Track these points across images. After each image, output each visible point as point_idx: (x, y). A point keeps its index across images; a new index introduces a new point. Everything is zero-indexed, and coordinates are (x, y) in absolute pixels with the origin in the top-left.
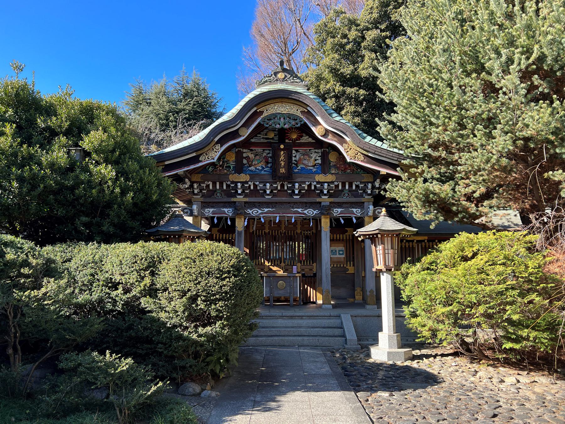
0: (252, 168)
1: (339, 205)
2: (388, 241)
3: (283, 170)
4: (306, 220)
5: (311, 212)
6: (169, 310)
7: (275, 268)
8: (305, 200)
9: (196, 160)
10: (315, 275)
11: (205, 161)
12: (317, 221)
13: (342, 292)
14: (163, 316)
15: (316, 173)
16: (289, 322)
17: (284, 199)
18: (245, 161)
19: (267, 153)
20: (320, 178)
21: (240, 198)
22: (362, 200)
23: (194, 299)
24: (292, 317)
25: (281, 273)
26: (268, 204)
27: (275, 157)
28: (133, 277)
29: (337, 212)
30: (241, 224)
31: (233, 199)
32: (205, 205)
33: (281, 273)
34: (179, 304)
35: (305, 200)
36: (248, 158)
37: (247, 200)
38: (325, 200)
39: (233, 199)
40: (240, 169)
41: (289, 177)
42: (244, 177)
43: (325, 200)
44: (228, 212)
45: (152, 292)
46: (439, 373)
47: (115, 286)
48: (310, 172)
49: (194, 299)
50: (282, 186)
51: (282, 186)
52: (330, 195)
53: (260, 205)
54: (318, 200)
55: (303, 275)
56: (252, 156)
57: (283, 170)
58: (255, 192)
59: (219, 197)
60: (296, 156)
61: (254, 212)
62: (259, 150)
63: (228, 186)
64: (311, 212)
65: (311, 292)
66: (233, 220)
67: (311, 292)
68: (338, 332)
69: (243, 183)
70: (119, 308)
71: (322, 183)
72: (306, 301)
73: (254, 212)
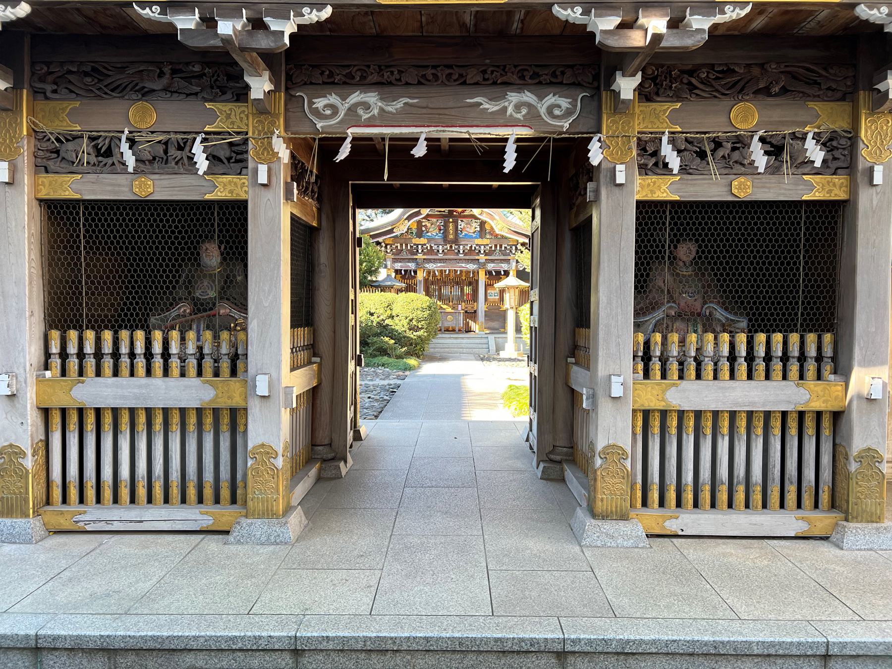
0: (429, 234)
1: (493, 261)
2: (512, 291)
3: (451, 237)
4: (468, 272)
5: (471, 267)
6: (400, 325)
7: (444, 307)
8: (467, 257)
9: (391, 231)
10: (475, 312)
11: (397, 232)
12: (475, 273)
13: (495, 324)
14: (397, 328)
15: (476, 238)
16: (455, 341)
17: (452, 257)
18: (424, 229)
19: (440, 222)
20: (479, 241)
21: (420, 256)
22: (509, 258)
23: (411, 320)
24: (456, 338)
25: (450, 310)
26: (440, 260)
27: (446, 226)
28: (382, 311)
29: (490, 266)
30: (421, 275)
31: (415, 257)
32: (395, 261)
33: (450, 310)
34: (405, 322)
35: (467, 257)
36: (425, 226)
37: (425, 257)
38: (482, 258)
39: (415, 257)
40: (420, 234)
41: (456, 241)
42: (423, 241)
43: (482, 258)
44: (412, 266)
45: (392, 317)
46: (359, 242)
47: (372, 314)
48: (471, 237)
49: (411, 320)
50: (451, 247)
51: (451, 247)
52: (486, 254)
53: (435, 261)
54: (477, 257)
55: (466, 312)
56: (429, 225)
57: (451, 237)
58: (431, 251)
59: (405, 255)
60: (461, 225)
61: (430, 266)
62: (435, 220)
63: (411, 247)
64: (471, 267)
65: (472, 324)
66: (415, 272)
67: (472, 324)
68: (485, 346)
69: (422, 245)
70: (374, 324)
71: (480, 246)
72: (468, 330)
73: (430, 266)
